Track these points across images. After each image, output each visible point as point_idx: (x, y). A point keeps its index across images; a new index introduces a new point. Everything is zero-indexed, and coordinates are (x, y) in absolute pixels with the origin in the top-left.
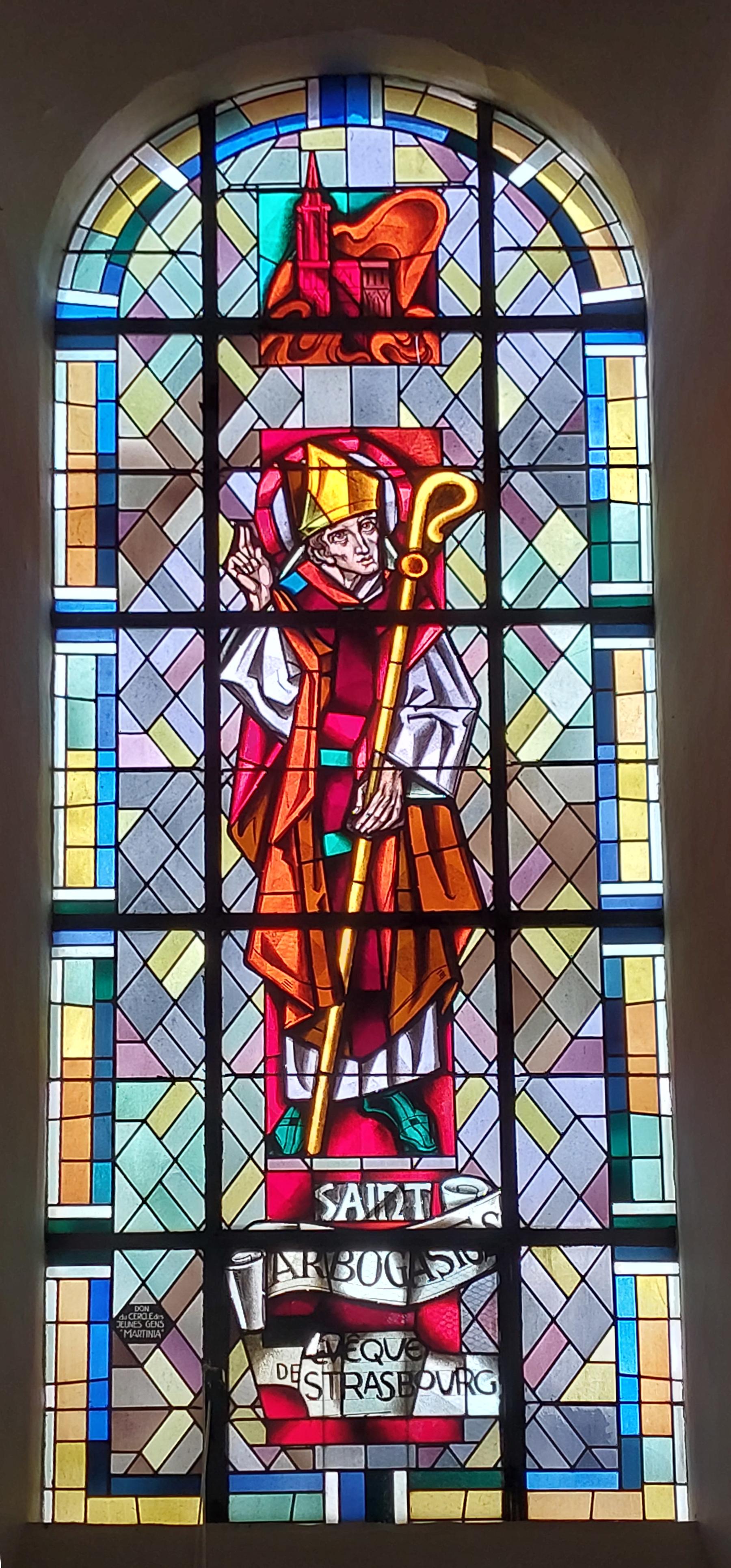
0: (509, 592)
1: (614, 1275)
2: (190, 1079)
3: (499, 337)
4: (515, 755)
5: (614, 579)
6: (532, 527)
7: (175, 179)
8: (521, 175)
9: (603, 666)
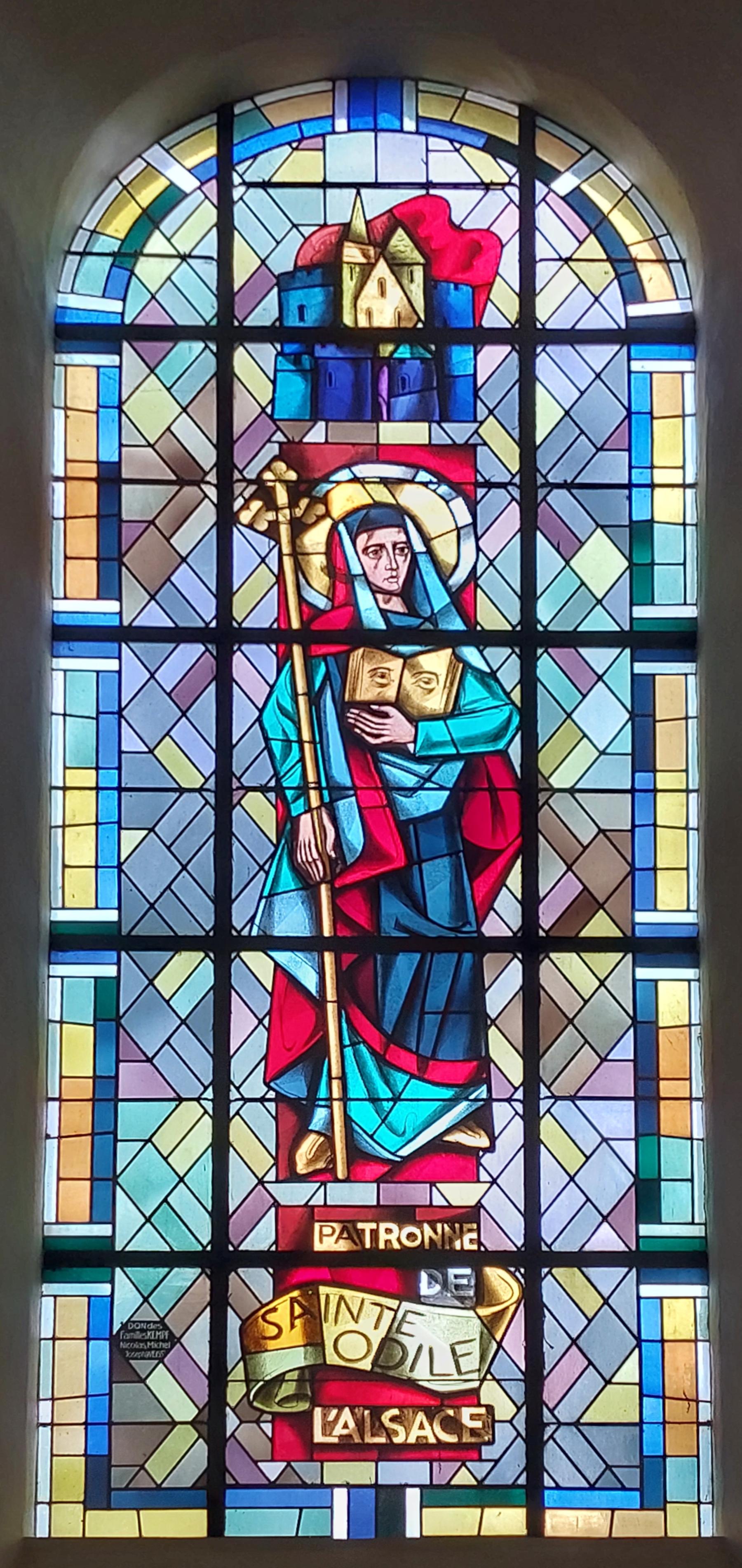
0: (544, 612)
1: (639, 1298)
2: (200, 790)
3: (539, 349)
4: (547, 780)
5: (656, 602)
6: (569, 546)
7: (187, 183)
8: (565, 184)
9: (643, 689)
